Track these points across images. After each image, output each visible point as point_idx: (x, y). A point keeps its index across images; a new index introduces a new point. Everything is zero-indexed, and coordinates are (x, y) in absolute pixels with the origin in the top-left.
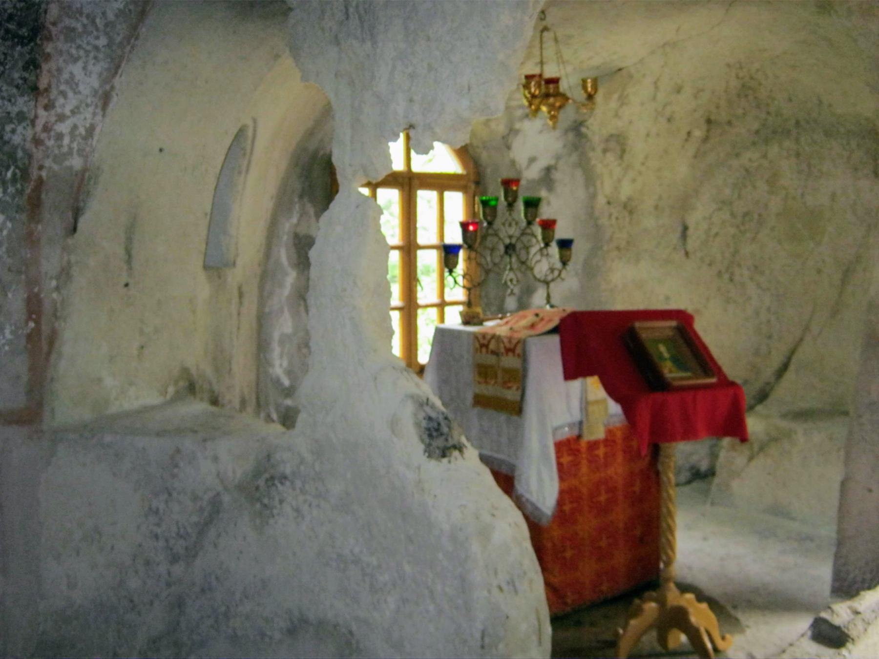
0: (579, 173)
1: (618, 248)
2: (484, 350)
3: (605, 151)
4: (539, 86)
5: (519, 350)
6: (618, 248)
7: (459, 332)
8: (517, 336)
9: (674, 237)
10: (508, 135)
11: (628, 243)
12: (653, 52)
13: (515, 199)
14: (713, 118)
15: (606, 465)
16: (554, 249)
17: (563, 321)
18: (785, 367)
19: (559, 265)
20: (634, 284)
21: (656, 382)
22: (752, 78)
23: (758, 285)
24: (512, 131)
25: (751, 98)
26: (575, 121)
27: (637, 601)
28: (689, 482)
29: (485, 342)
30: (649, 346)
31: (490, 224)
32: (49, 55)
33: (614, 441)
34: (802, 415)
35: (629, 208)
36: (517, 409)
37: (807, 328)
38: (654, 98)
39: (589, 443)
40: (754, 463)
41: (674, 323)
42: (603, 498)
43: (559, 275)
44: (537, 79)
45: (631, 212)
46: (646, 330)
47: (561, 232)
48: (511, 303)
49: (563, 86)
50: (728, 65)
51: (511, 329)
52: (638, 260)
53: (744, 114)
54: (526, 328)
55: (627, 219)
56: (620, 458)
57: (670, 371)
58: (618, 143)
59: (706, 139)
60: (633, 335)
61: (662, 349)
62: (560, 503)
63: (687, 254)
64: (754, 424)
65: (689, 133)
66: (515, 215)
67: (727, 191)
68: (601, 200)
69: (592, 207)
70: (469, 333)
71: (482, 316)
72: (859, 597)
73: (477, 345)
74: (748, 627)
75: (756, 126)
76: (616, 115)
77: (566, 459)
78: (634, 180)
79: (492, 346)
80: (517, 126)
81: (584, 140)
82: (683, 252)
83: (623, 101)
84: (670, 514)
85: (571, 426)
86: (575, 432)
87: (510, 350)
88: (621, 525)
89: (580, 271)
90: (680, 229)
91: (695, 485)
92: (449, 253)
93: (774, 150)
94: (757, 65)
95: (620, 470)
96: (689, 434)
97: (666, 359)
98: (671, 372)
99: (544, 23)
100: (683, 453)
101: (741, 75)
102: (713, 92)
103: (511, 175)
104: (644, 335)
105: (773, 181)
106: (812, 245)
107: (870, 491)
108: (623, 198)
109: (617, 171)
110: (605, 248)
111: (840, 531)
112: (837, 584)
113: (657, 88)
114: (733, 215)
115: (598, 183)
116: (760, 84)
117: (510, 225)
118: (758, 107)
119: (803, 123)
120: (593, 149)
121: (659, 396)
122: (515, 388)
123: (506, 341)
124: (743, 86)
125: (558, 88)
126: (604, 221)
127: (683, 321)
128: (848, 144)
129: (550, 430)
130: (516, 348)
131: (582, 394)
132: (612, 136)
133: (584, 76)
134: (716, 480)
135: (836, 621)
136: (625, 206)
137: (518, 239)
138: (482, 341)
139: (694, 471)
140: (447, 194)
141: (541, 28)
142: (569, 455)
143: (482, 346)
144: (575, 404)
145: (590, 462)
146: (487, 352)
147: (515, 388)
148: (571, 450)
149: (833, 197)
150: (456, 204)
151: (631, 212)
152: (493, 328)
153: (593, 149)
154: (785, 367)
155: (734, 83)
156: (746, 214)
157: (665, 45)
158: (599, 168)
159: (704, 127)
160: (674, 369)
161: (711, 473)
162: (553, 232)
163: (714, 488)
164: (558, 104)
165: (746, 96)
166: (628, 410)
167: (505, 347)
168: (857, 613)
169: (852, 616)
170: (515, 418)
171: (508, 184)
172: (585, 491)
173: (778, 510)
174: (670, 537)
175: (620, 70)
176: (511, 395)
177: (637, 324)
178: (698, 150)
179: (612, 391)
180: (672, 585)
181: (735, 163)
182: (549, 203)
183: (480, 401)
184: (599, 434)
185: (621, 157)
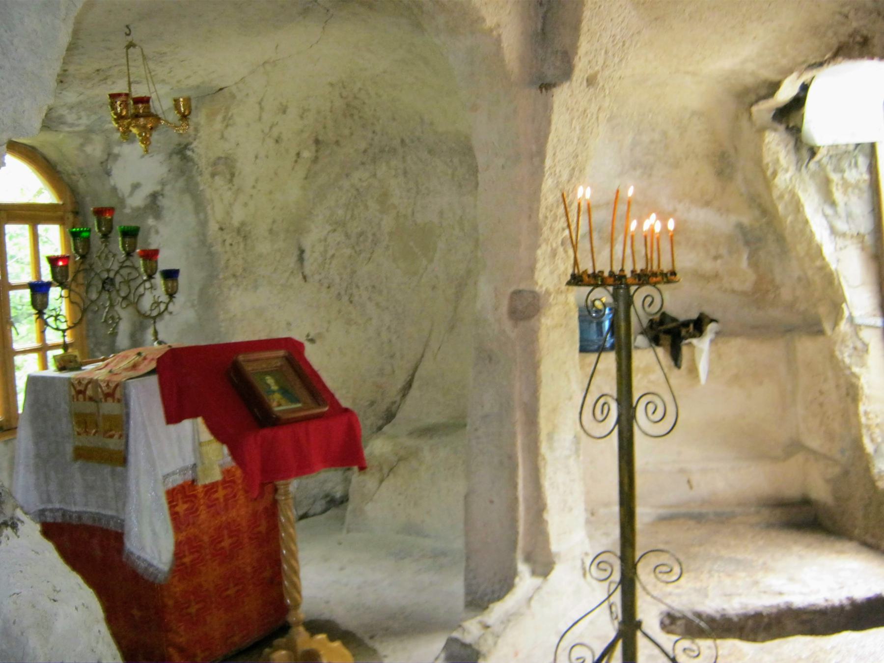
0: (187, 199)
1: (234, 276)
2: (81, 396)
3: (213, 175)
4: (125, 105)
5: (118, 395)
6: (234, 276)
7: (53, 378)
8: (117, 379)
9: (291, 261)
10: (107, 160)
11: (244, 270)
12: (253, 72)
13: (110, 229)
14: (320, 138)
15: (226, 508)
16: (159, 280)
17: (160, 361)
18: (409, 385)
19: (164, 298)
20: (251, 313)
21: (264, 418)
22: (355, 98)
23: (377, 305)
24: (111, 156)
25: (356, 117)
26: (179, 145)
27: (267, 650)
28: (324, 511)
29: (81, 388)
30: (256, 381)
31: (83, 257)
32: (807, 191)
33: (233, 482)
34: (428, 432)
35: (243, 233)
36: (121, 459)
37: (426, 345)
38: (260, 119)
39: (205, 486)
40: (384, 484)
41: (282, 353)
42: (226, 543)
43: (166, 309)
44: (123, 98)
45: (245, 238)
46: (250, 364)
47: (164, 263)
48: (123, 340)
49: (156, 106)
50: (332, 85)
51: (110, 371)
52: (256, 288)
53: (352, 134)
54: (126, 369)
55: (242, 246)
56: (241, 498)
57: (279, 405)
58: (226, 166)
59: (315, 160)
60: (237, 369)
61: (270, 380)
62: (178, 555)
63: (305, 278)
64: (376, 448)
65: (298, 154)
66: (112, 247)
67: (340, 212)
68: (213, 227)
69: (204, 235)
70: (60, 379)
71: (79, 359)
72: (489, 610)
73: (73, 393)
74: (385, 656)
75: (363, 145)
76: (222, 137)
77: (182, 508)
78: (246, 205)
79: (89, 393)
80: (116, 150)
81: (190, 164)
82: (301, 276)
83: (228, 121)
84: (293, 554)
85: (183, 471)
86: (189, 476)
87: (110, 395)
88: (249, 569)
89: (196, 302)
90: (296, 253)
91: (332, 512)
92: (39, 290)
93: (382, 170)
94: (359, 85)
95: (243, 512)
96: (304, 468)
97: (274, 392)
98: (279, 405)
99: (129, 38)
100: (296, 488)
101: (345, 94)
102: (319, 112)
103: (105, 203)
104: (249, 368)
105: (384, 198)
106: (425, 262)
107: (492, 502)
108: (236, 222)
109: (228, 195)
110: (221, 276)
111: (467, 544)
112: (469, 599)
113: (262, 109)
114: (347, 236)
115: (209, 208)
116: (364, 103)
117: (107, 258)
118: (364, 126)
119: (407, 141)
120: (201, 174)
121: (267, 432)
122: (116, 436)
123: (103, 385)
124: (348, 105)
125: (149, 108)
126: (218, 248)
127: (292, 351)
128: (451, 161)
129: (160, 477)
130: (115, 392)
131: (194, 436)
132: (219, 158)
133: (176, 96)
134: (350, 506)
135: (468, 639)
136: (239, 231)
137: (117, 272)
138: (79, 388)
139: (328, 499)
140: (41, 228)
141: (126, 44)
142: (186, 502)
143: (79, 392)
144: (188, 447)
145: (209, 507)
146: (85, 400)
147: (116, 436)
148: (187, 496)
149: (441, 213)
150: (53, 239)
151: (245, 238)
152: (91, 371)
153: (201, 174)
154: (409, 385)
155: (339, 103)
156: (361, 234)
157: (265, 63)
158: (208, 194)
159: (313, 148)
160: (283, 402)
161: (344, 500)
162: (156, 262)
163: (349, 517)
164: (149, 126)
165: (352, 115)
166: (235, 452)
167: (103, 391)
168: (487, 627)
169: (483, 632)
170: (119, 469)
171: (99, 212)
172: (206, 538)
173: (411, 529)
174: (295, 579)
175: (221, 89)
176: (113, 444)
177: (241, 358)
178: (309, 170)
179: (219, 432)
180: (301, 629)
181: (346, 183)
182: (157, 232)
183: (81, 454)
184: (216, 476)
185: (231, 181)
